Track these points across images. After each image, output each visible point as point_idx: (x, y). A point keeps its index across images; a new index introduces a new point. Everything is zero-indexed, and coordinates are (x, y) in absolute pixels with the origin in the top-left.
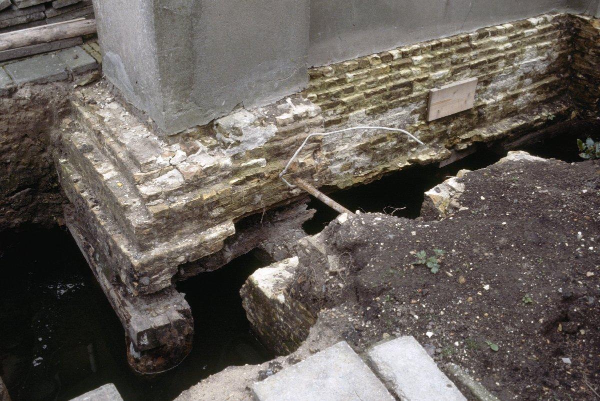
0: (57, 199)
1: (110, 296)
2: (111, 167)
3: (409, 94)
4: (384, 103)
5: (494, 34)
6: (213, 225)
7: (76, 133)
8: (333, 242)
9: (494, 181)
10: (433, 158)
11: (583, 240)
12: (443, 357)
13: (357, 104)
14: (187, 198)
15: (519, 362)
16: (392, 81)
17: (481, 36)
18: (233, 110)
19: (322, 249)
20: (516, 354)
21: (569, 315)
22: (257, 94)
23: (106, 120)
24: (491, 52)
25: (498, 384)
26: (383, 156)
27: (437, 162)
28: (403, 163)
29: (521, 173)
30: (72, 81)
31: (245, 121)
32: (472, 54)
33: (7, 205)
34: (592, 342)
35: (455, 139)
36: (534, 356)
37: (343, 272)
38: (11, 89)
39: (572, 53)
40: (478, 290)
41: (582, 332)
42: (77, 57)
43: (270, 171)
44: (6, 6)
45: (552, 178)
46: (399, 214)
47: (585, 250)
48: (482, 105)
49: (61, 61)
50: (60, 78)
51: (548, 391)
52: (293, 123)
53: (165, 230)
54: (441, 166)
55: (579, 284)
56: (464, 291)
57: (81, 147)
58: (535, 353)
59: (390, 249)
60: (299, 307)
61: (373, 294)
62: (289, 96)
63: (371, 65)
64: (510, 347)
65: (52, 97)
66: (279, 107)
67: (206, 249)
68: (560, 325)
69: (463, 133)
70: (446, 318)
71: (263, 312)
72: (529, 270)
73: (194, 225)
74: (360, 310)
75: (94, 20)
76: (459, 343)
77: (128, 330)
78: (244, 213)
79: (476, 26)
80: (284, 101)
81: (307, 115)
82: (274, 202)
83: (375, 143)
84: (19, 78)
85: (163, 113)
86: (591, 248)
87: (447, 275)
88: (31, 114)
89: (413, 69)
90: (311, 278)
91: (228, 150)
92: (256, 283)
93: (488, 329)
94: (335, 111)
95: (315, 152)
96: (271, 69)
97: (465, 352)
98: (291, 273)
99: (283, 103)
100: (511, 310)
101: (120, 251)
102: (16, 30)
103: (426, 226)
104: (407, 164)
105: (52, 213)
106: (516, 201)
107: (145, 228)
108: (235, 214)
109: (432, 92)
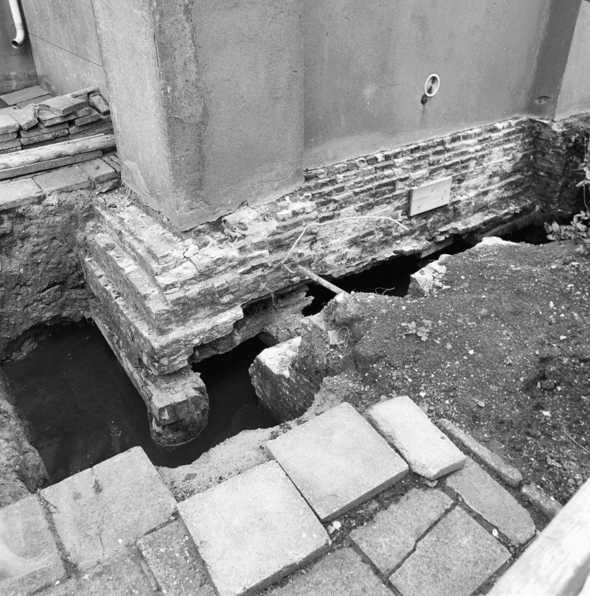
0: (83, 294)
1: (133, 378)
2: (132, 262)
3: (392, 192)
4: (371, 200)
5: (465, 138)
6: (223, 311)
7: (100, 234)
8: (332, 318)
9: (472, 262)
10: (416, 249)
11: (555, 308)
12: (436, 414)
13: (347, 202)
14: (200, 286)
15: (504, 416)
16: (377, 180)
17: (454, 140)
18: (238, 208)
19: (323, 326)
20: (501, 409)
21: (546, 373)
22: (259, 194)
23: (125, 221)
24: (463, 153)
25: (486, 435)
26: (371, 249)
27: (419, 253)
28: (389, 254)
29: (495, 255)
30: (94, 188)
31: (249, 217)
32: (447, 155)
33: (39, 301)
34: (568, 397)
35: (434, 232)
36: (517, 410)
37: (342, 345)
38: (40, 196)
39: (534, 154)
40: (464, 355)
41: (559, 388)
42: (98, 168)
43: (273, 261)
44: (33, 124)
45: (524, 258)
46: (389, 294)
47: (557, 317)
48: (456, 202)
49: (84, 171)
50: (84, 186)
51: (532, 440)
52: (292, 218)
53: (181, 316)
54: (423, 256)
55: (553, 346)
56: (451, 356)
57: (104, 246)
58: (517, 408)
59: (383, 322)
60: (303, 381)
61: (370, 362)
62: (287, 195)
63: (358, 167)
64: (495, 403)
65: (77, 203)
66: (279, 204)
67: (218, 332)
68: (539, 383)
69: (441, 227)
70: (437, 380)
71: (271, 388)
72: (508, 335)
74: (359, 377)
75: (112, 136)
76: (450, 401)
77: (150, 407)
78: (250, 299)
79: (449, 130)
80: (283, 198)
81: (304, 212)
82: (277, 289)
83: (364, 236)
84: (47, 187)
85: (177, 211)
86: (563, 315)
87: (436, 343)
88: (58, 219)
89: (395, 170)
90: (314, 352)
91: (235, 243)
92: (263, 361)
93: (474, 388)
94: (328, 208)
95: (312, 243)
96: (271, 170)
97: (455, 409)
98: (295, 351)
99: (282, 200)
100: (494, 371)
101: (141, 335)
102: (44, 145)
103: (414, 301)
104: (393, 254)
105: (79, 308)
106: (492, 278)
107: (164, 314)
108: (243, 300)
109: (413, 190)
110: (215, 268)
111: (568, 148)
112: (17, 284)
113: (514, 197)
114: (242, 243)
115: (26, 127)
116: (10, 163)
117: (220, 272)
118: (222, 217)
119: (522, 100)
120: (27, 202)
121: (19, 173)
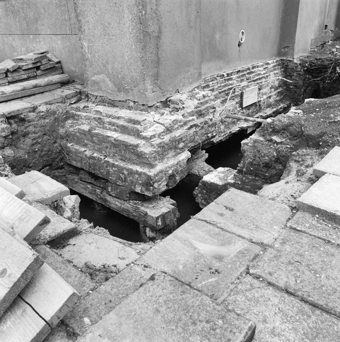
5: (258, 67)
6: (180, 153)
17: (253, 68)
24: (259, 74)
32: (253, 75)
60: (248, 179)
65: (58, 110)
73: (171, 153)
91: (179, 111)
96: (188, 72)
110: (173, 126)
111: (304, 70)
112: (24, 166)
113: (281, 100)
114: (183, 112)
115: (11, 70)
116: (4, 91)
117: (176, 129)
118: (168, 98)
119: (275, 49)
120: (26, 111)
121: (11, 98)
